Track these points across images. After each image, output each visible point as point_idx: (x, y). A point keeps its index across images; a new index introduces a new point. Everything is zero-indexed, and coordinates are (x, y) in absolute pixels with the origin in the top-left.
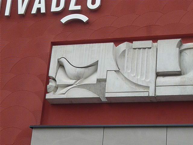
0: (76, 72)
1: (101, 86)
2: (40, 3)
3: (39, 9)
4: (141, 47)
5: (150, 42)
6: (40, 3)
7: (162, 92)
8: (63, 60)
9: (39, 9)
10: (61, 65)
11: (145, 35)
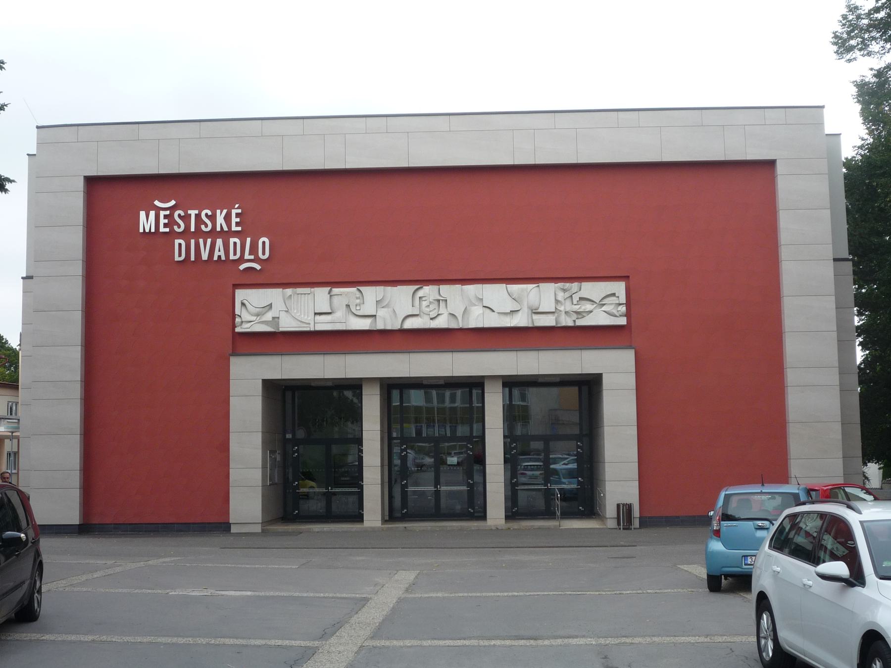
2: (219, 251)
3: (219, 257)
6: (219, 251)
9: (219, 257)
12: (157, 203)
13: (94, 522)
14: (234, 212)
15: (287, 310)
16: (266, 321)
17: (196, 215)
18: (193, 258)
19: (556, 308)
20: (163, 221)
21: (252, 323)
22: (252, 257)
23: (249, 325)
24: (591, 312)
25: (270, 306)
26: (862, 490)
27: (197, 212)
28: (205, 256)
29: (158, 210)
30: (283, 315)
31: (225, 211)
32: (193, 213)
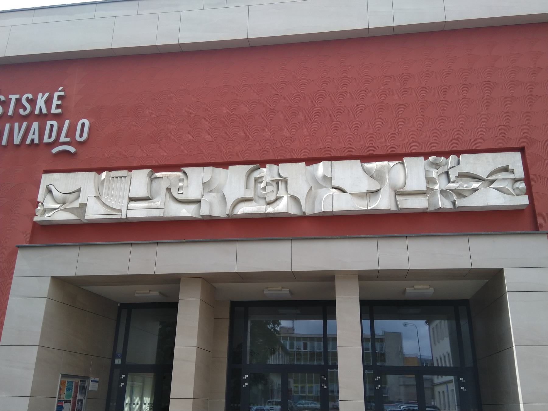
2: (34, 134)
3: (33, 140)
6: (34, 134)
9: (33, 140)
14: (56, 95)
19: (427, 188)
24: (476, 190)
31: (47, 94)
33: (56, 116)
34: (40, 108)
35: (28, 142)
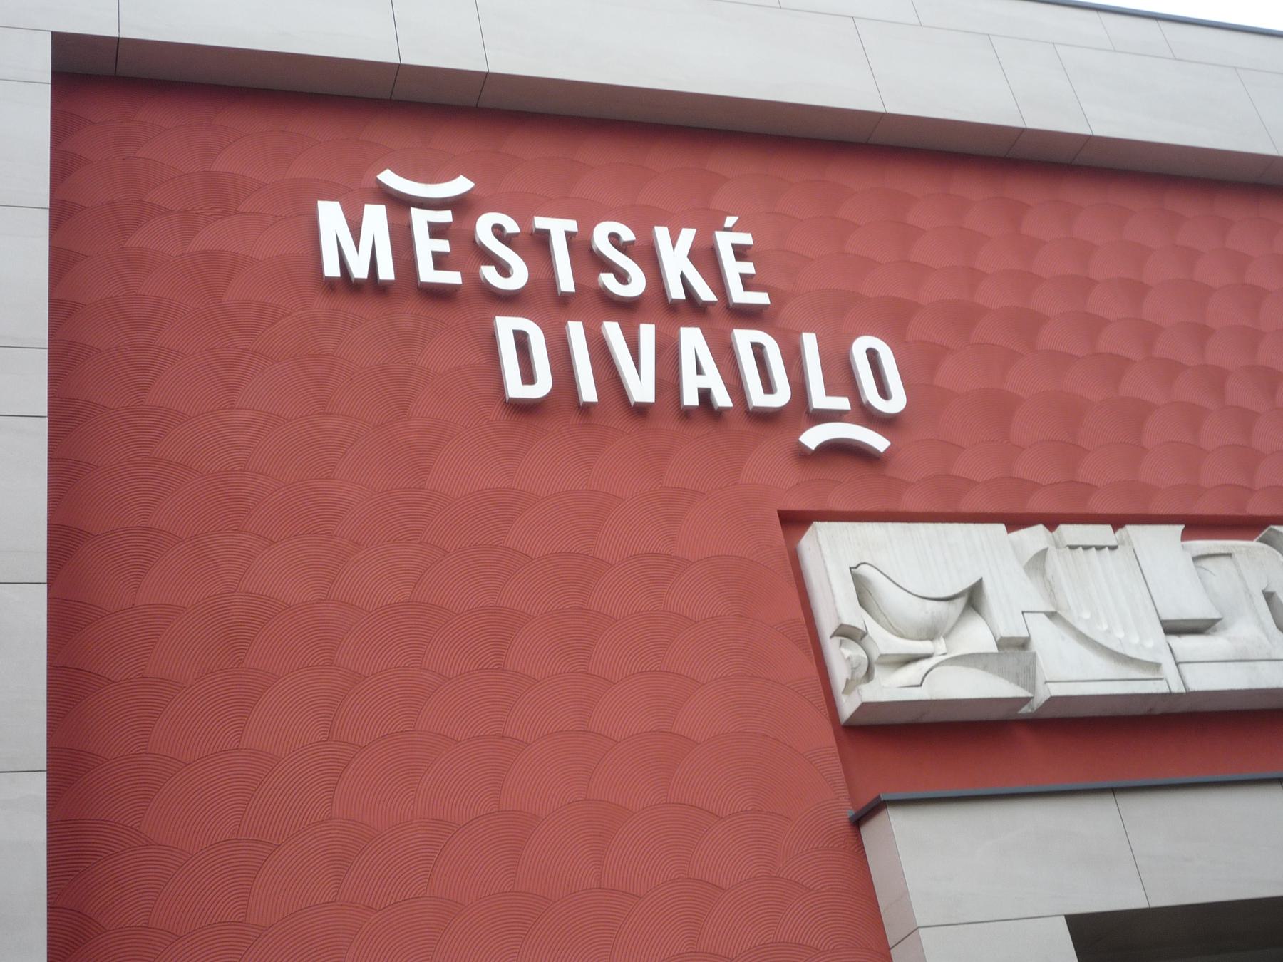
0: (927, 613)
1: (1019, 661)
2: (699, 371)
3: (705, 395)
4: (1088, 543)
5: (1040, 529)
6: (699, 371)
7: (1169, 682)
8: (865, 571)
9: (705, 395)
10: (863, 592)
11: (990, 508)
12: (389, 178)
13: (819, 533)
14: (725, 242)
15: (1052, 609)
16: (980, 655)
17: (569, 235)
18: (588, 392)
20: (426, 247)
21: (925, 665)
22: (843, 403)
23: (912, 673)
25: (973, 599)
26: (1186, 536)
27: (572, 226)
28: (642, 388)
29: (399, 204)
30: (1045, 638)
31: (688, 236)
32: (558, 228)
33: (749, 316)
34: (683, 276)
35: (690, 398)
